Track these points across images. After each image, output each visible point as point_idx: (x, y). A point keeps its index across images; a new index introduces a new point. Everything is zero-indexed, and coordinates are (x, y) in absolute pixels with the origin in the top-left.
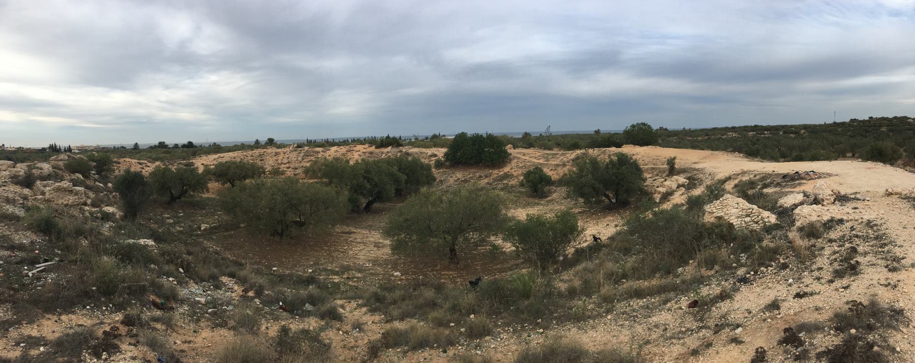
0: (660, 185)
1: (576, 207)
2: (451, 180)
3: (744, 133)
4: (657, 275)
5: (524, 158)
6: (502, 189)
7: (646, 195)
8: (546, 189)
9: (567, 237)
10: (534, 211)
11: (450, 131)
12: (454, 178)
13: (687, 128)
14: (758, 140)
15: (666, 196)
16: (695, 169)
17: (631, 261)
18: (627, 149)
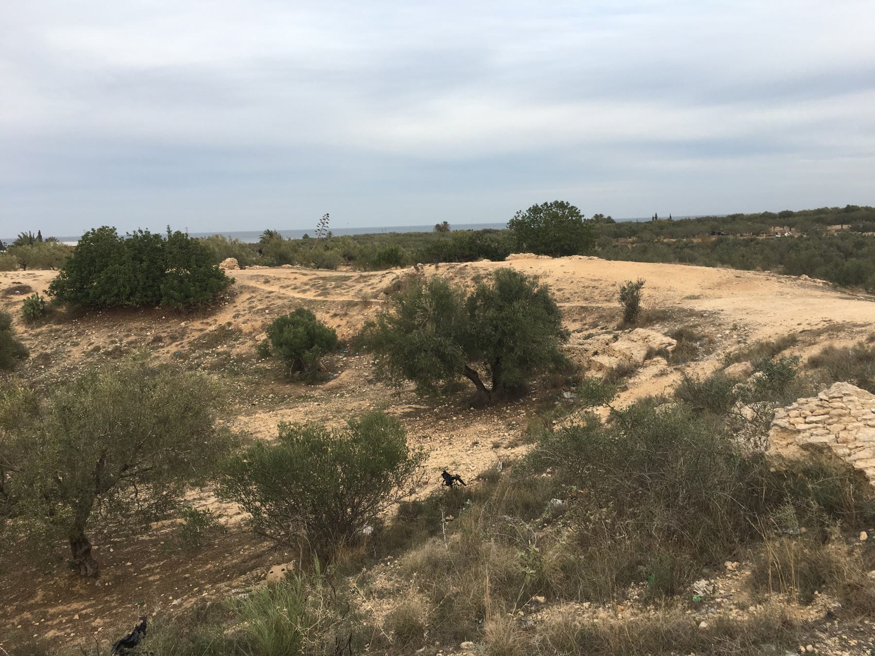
0: (599, 350)
1: (398, 400)
2: (76, 353)
3: (817, 227)
4: (634, 592)
5: (267, 288)
6: (213, 368)
7: (566, 375)
8: (324, 360)
9: (379, 476)
10: (296, 415)
11: (69, 229)
12: (86, 345)
13: (663, 215)
14: (859, 245)
15: (623, 373)
16: (692, 313)
17: (557, 545)
18: (523, 264)
